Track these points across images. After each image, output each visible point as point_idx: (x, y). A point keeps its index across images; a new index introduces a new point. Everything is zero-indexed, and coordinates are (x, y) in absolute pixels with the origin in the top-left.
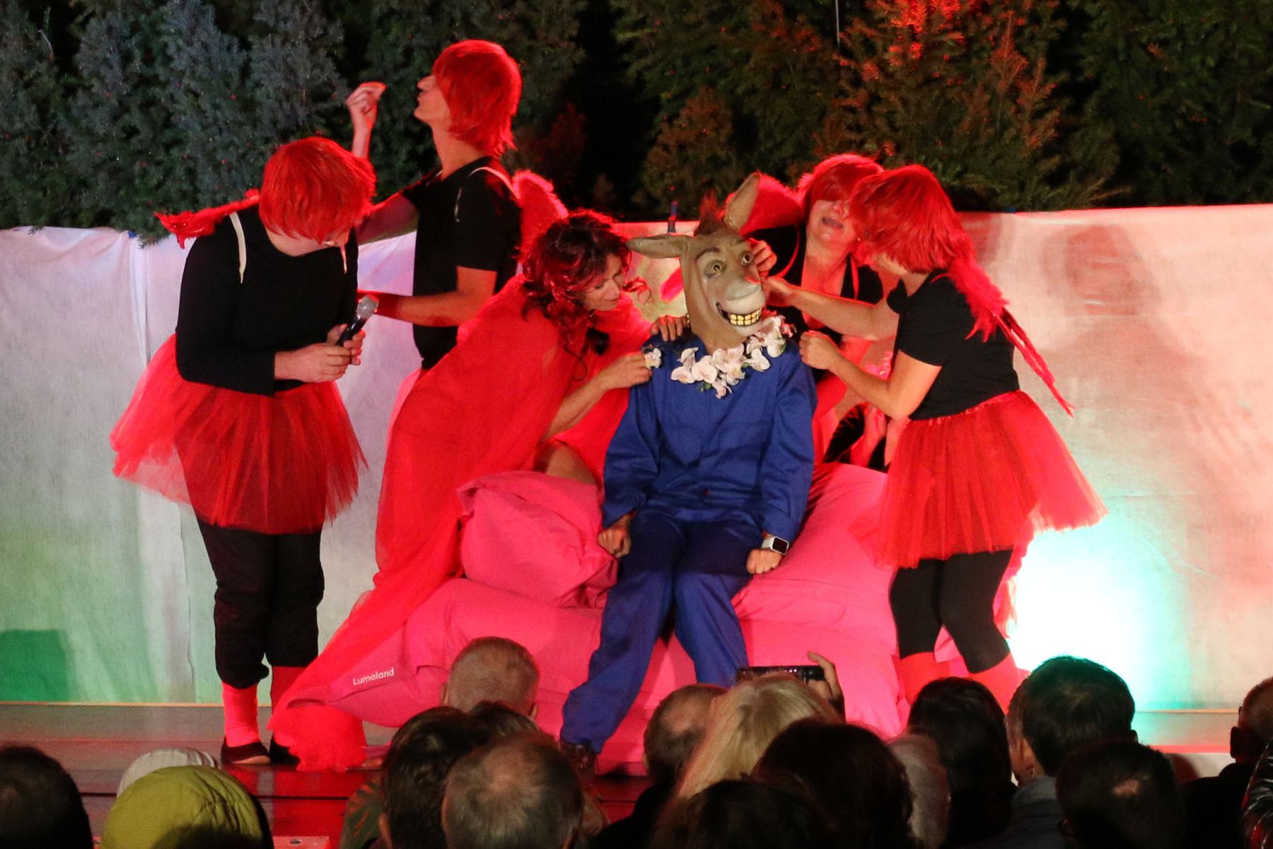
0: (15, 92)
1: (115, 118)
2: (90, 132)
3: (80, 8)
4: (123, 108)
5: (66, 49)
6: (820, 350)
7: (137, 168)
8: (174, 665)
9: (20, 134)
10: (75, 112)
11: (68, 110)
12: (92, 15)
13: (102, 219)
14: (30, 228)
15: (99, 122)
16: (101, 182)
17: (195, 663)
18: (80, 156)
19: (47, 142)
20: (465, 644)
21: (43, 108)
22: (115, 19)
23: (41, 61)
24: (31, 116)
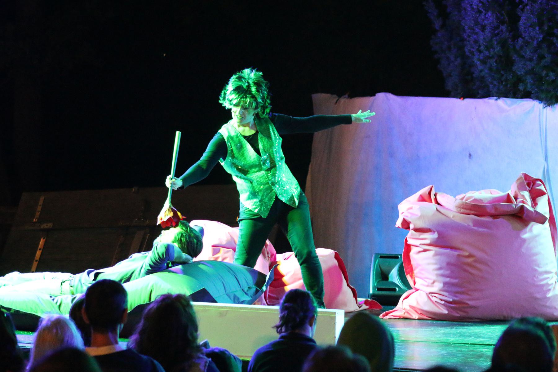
0: (492, 38)
1: (535, 50)
2: (523, 57)
3: (521, 2)
4: (539, 46)
5: (514, 20)
6: (23, 336)
7: (544, 73)
8: (441, 300)
9: (492, 57)
10: (517, 47)
11: (514, 46)
12: (527, 5)
13: (527, 95)
14: (495, 98)
15: (528, 53)
16: (529, 80)
17: (314, 333)
18: (520, 68)
19: (506, 62)
20: (396, 341)
21: (503, 44)
22: (536, 6)
23: (503, 25)
24: (498, 49)
